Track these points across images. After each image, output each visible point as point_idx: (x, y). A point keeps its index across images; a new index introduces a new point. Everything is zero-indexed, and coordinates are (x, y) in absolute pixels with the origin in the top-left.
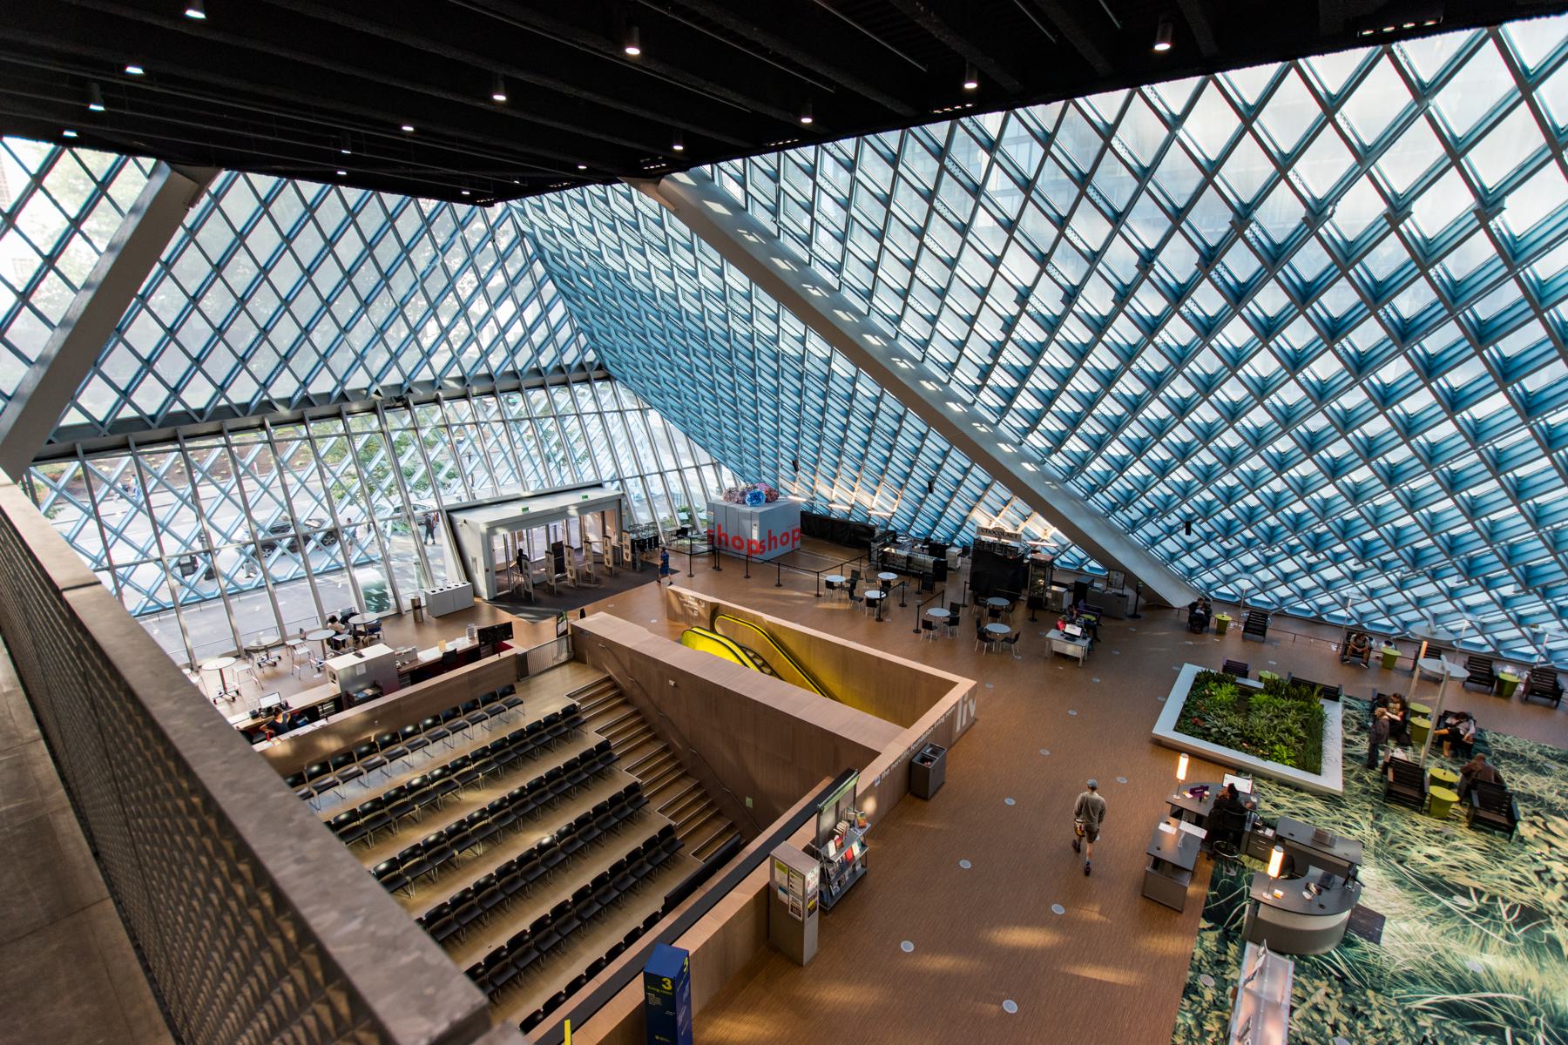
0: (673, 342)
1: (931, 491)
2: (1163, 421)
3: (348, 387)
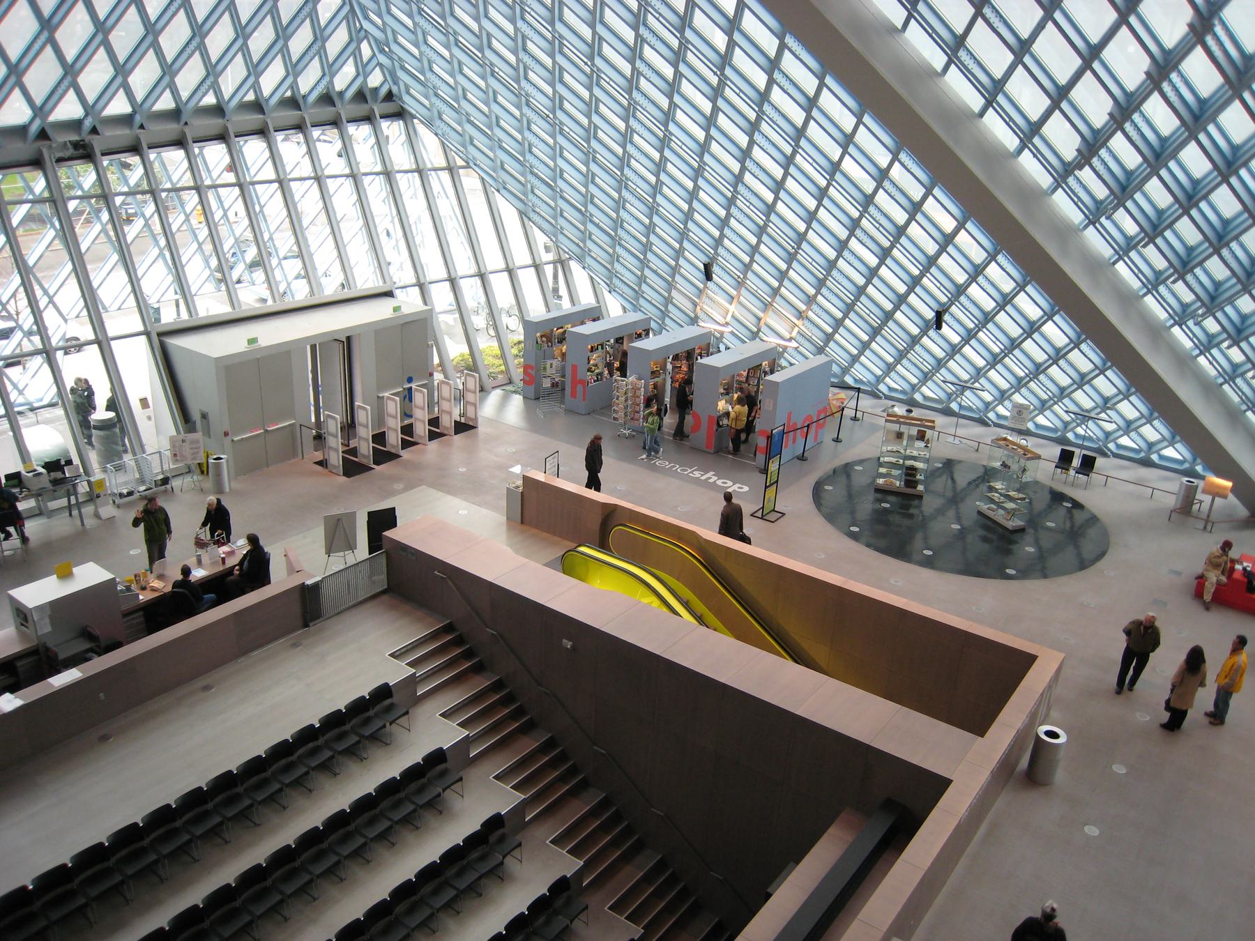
0: (428, 51)
1: (939, 327)
2: (1190, 250)
3: (53, 117)
